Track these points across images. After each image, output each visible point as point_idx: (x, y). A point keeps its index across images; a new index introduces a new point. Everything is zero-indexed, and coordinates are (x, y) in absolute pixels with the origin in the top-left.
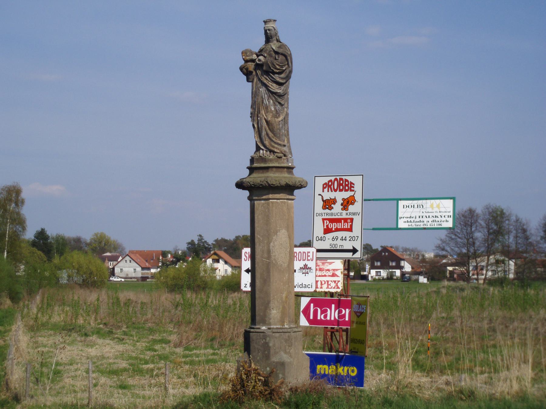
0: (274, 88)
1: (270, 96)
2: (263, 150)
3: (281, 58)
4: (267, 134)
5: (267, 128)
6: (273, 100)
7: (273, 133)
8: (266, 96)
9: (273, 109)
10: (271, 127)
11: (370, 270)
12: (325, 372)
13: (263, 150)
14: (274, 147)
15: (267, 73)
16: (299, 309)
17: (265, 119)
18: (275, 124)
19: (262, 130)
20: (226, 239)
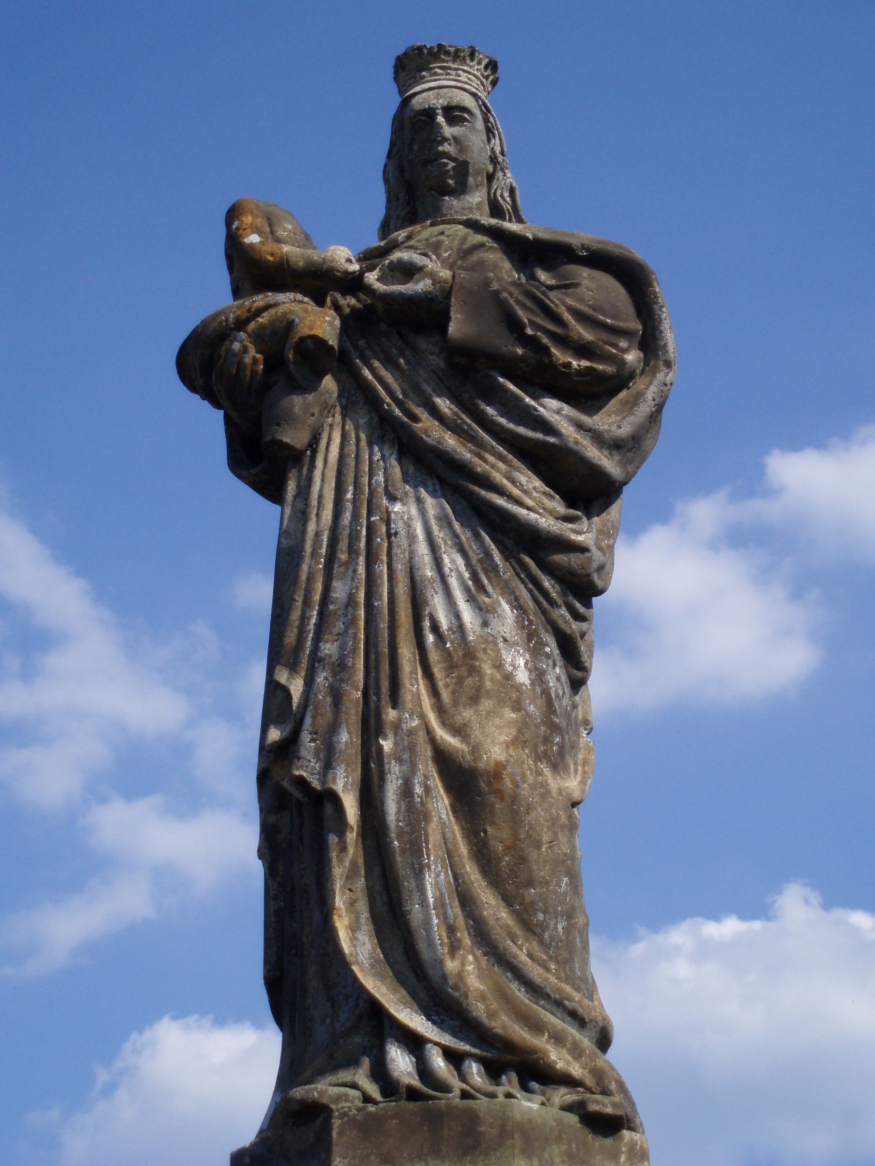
0: (535, 503)
1: (492, 570)
2: (414, 1043)
3: (595, 287)
4: (466, 899)
5: (463, 849)
6: (517, 605)
7: (508, 900)
8: (453, 561)
9: (523, 677)
10: (498, 836)
11: (403, 242)
12: (508, 1077)
13: (414, 1043)
14: (537, 1027)
15: (469, 374)
16: (428, 906)
17: (443, 759)
18: (539, 815)
19: (415, 848)
20: (206, 404)
